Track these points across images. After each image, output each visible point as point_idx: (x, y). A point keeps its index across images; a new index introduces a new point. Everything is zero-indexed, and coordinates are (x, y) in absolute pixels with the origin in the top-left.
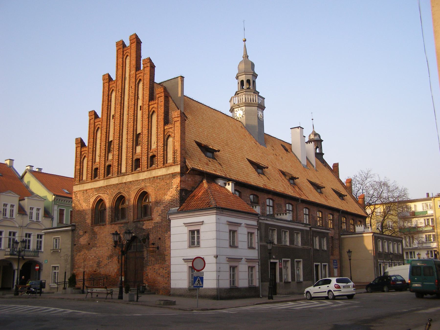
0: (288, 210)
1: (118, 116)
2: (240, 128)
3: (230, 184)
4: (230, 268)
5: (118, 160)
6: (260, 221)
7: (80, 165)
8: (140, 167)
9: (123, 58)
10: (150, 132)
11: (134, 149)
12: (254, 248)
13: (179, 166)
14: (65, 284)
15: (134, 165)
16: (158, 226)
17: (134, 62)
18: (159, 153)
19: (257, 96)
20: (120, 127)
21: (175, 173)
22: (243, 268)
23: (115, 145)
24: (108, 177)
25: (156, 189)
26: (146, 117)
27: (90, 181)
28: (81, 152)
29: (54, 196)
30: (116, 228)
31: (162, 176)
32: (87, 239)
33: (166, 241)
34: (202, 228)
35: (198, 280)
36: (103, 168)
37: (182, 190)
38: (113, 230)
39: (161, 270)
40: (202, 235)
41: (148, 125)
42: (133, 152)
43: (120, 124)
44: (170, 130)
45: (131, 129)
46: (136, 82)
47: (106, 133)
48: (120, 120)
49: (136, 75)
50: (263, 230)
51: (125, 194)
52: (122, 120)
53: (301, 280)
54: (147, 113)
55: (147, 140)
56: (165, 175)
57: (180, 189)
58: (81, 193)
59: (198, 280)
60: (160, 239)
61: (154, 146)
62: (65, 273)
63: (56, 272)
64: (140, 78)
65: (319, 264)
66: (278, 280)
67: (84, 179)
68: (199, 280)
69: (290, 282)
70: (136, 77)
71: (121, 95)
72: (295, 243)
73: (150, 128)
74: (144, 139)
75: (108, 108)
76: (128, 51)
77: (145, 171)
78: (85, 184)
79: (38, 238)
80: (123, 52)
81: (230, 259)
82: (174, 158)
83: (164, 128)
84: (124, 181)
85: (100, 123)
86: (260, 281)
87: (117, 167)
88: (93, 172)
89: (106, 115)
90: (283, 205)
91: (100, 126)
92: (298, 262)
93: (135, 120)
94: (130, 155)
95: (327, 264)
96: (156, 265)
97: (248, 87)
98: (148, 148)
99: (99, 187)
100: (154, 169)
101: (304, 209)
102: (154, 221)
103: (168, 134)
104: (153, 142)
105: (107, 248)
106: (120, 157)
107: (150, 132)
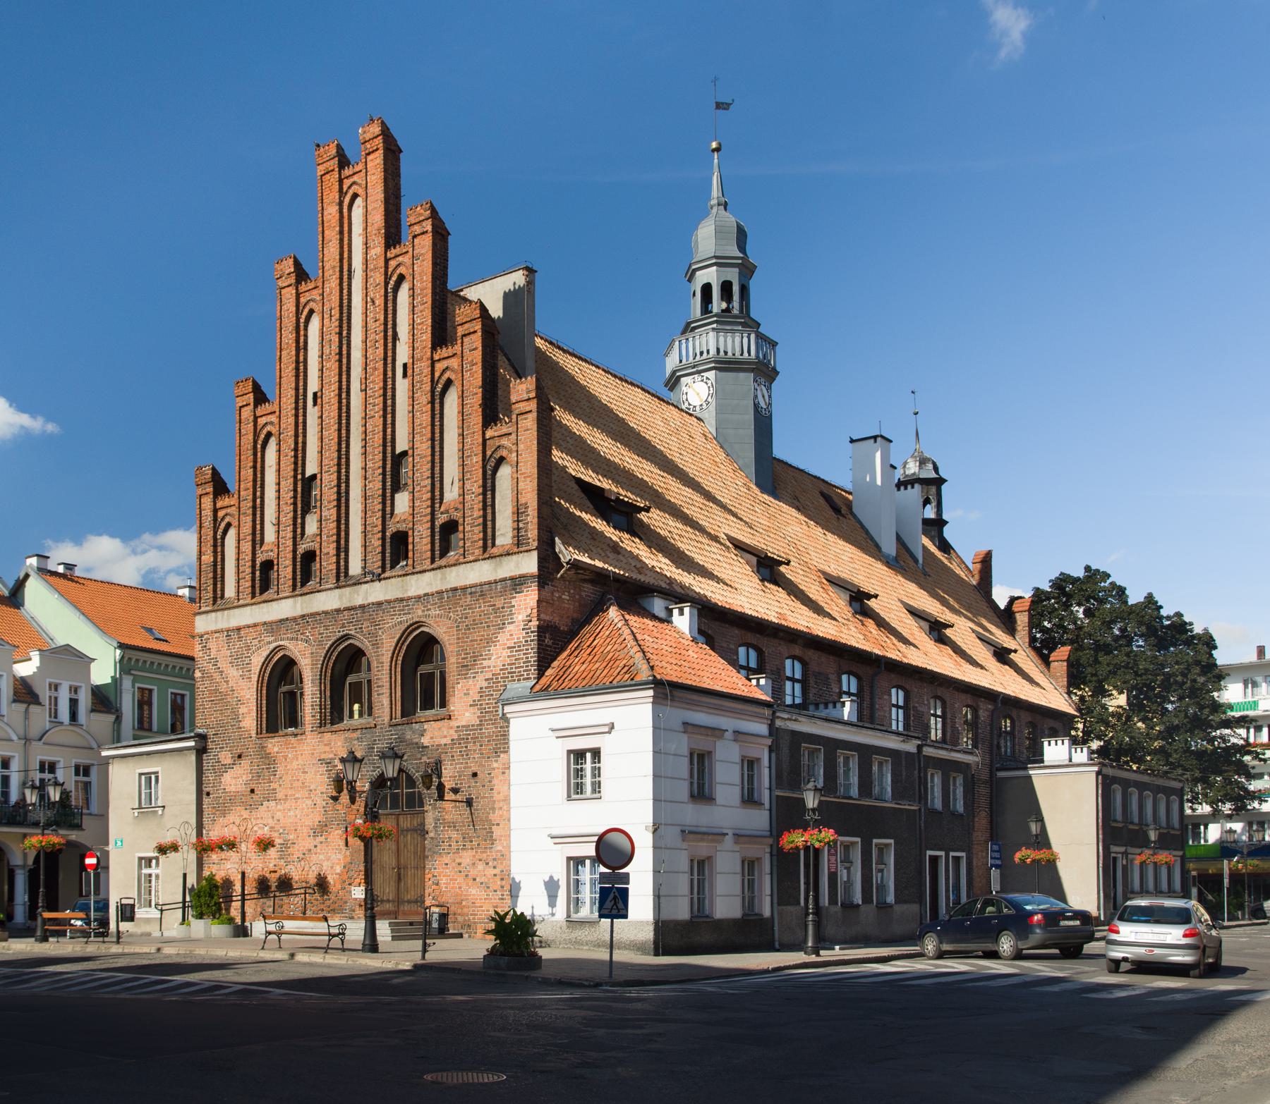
0: (845, 693)
1: (330, 395)
2: (699, 439)
3: (687, 610)
4: (743, 862)
5: (338, 535)
6: (778, 723)
7: (215, 552)
8: (406, 557)
9: (341, 204)
10: (437, 449)
11: (388, 502)
12: (759, 804)
13: (535, 554)
14: (184, 908)
15: (388, 551)
16: (467, 737)
17: (378, 218)
18: (468, 513)
19: (753, 336)
20: (339, 430)
21: (521, 576)
22: (727, 866)
23: (325, 490)
24: (305, 590)
25: (463, 626)
26: (423, 398)
27: (249, 601)
28: (215, 511)
29: (118, 652)
30: (337, 744)
31: (481, 585)
32: (244, 777)
33: (495, 781)
34: (606, 744)
35: (612, 896)
36: (289, 562)
37: (542, 630)
38: (327, 749)
39: (481, 866)
40: (606, 763)
41: (433, 425)
42: (384, 510)
43: (340, 423)
44: (504, 442)
45: (378, 438)
46: (386, 284)
47: (296, 450)
48: (340, 409)
49: (387, 261)
50: (785, 751)
51: (364, 643)
52: (344, 409)
53: (891, 898)
54: (428, 387)
55: (428, 474)
56: (489, 583)
57: (539, 627)
58: (223, 637)
59: (612, 896)
60: (475, 775)
61: (451, 494)
62: (185, 875)
63: (150, 875)
64: (402, 270)
65: (942, 853)
66: (825, 900)
67: (227, 595)
68: (615, 898)
69: (858, 906)
70: (386, 267)
71: (341, 326)
72: (876, 790)
73: (437, 435)
74: (417, 471)
75: (297, 369)
76: (355, 178)
77: (424, 571)
78: (232, 611)
79: (77, 773)
80: (341, 181)
81: (689, 833)
82: (518, 529)
83: (484, 434)
84: (359, 601)
85: (273, 418)
86: (775, 901)
87: (334, 559)
88: (258, 573)
89: (293, 392)
90: (833, 677)
91: (274, 430)
92: (881, 849)
93: (389, 409)
94: (376, 520)
95: (963, 854)
96: (464, 854)
97: (724, 305)
98: (433, 499)
99: (281, 621)
100: (455, 565)
101: (894, 691)
102: (454, 723)
103: (497, 456)
104: (447, 481)
105: (309, 802)
106: (343, 527)
107: (437, 449)
